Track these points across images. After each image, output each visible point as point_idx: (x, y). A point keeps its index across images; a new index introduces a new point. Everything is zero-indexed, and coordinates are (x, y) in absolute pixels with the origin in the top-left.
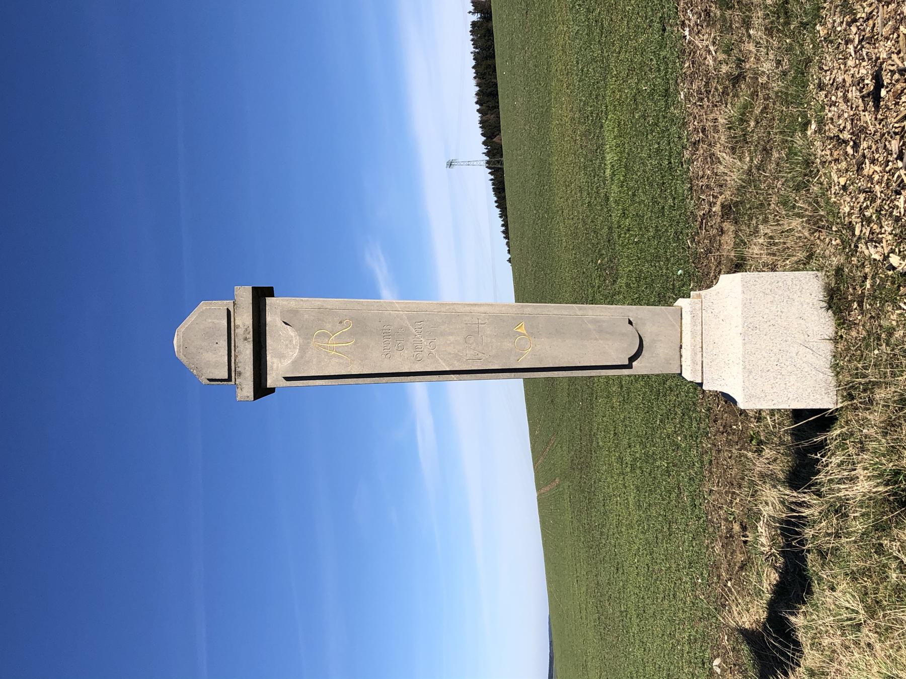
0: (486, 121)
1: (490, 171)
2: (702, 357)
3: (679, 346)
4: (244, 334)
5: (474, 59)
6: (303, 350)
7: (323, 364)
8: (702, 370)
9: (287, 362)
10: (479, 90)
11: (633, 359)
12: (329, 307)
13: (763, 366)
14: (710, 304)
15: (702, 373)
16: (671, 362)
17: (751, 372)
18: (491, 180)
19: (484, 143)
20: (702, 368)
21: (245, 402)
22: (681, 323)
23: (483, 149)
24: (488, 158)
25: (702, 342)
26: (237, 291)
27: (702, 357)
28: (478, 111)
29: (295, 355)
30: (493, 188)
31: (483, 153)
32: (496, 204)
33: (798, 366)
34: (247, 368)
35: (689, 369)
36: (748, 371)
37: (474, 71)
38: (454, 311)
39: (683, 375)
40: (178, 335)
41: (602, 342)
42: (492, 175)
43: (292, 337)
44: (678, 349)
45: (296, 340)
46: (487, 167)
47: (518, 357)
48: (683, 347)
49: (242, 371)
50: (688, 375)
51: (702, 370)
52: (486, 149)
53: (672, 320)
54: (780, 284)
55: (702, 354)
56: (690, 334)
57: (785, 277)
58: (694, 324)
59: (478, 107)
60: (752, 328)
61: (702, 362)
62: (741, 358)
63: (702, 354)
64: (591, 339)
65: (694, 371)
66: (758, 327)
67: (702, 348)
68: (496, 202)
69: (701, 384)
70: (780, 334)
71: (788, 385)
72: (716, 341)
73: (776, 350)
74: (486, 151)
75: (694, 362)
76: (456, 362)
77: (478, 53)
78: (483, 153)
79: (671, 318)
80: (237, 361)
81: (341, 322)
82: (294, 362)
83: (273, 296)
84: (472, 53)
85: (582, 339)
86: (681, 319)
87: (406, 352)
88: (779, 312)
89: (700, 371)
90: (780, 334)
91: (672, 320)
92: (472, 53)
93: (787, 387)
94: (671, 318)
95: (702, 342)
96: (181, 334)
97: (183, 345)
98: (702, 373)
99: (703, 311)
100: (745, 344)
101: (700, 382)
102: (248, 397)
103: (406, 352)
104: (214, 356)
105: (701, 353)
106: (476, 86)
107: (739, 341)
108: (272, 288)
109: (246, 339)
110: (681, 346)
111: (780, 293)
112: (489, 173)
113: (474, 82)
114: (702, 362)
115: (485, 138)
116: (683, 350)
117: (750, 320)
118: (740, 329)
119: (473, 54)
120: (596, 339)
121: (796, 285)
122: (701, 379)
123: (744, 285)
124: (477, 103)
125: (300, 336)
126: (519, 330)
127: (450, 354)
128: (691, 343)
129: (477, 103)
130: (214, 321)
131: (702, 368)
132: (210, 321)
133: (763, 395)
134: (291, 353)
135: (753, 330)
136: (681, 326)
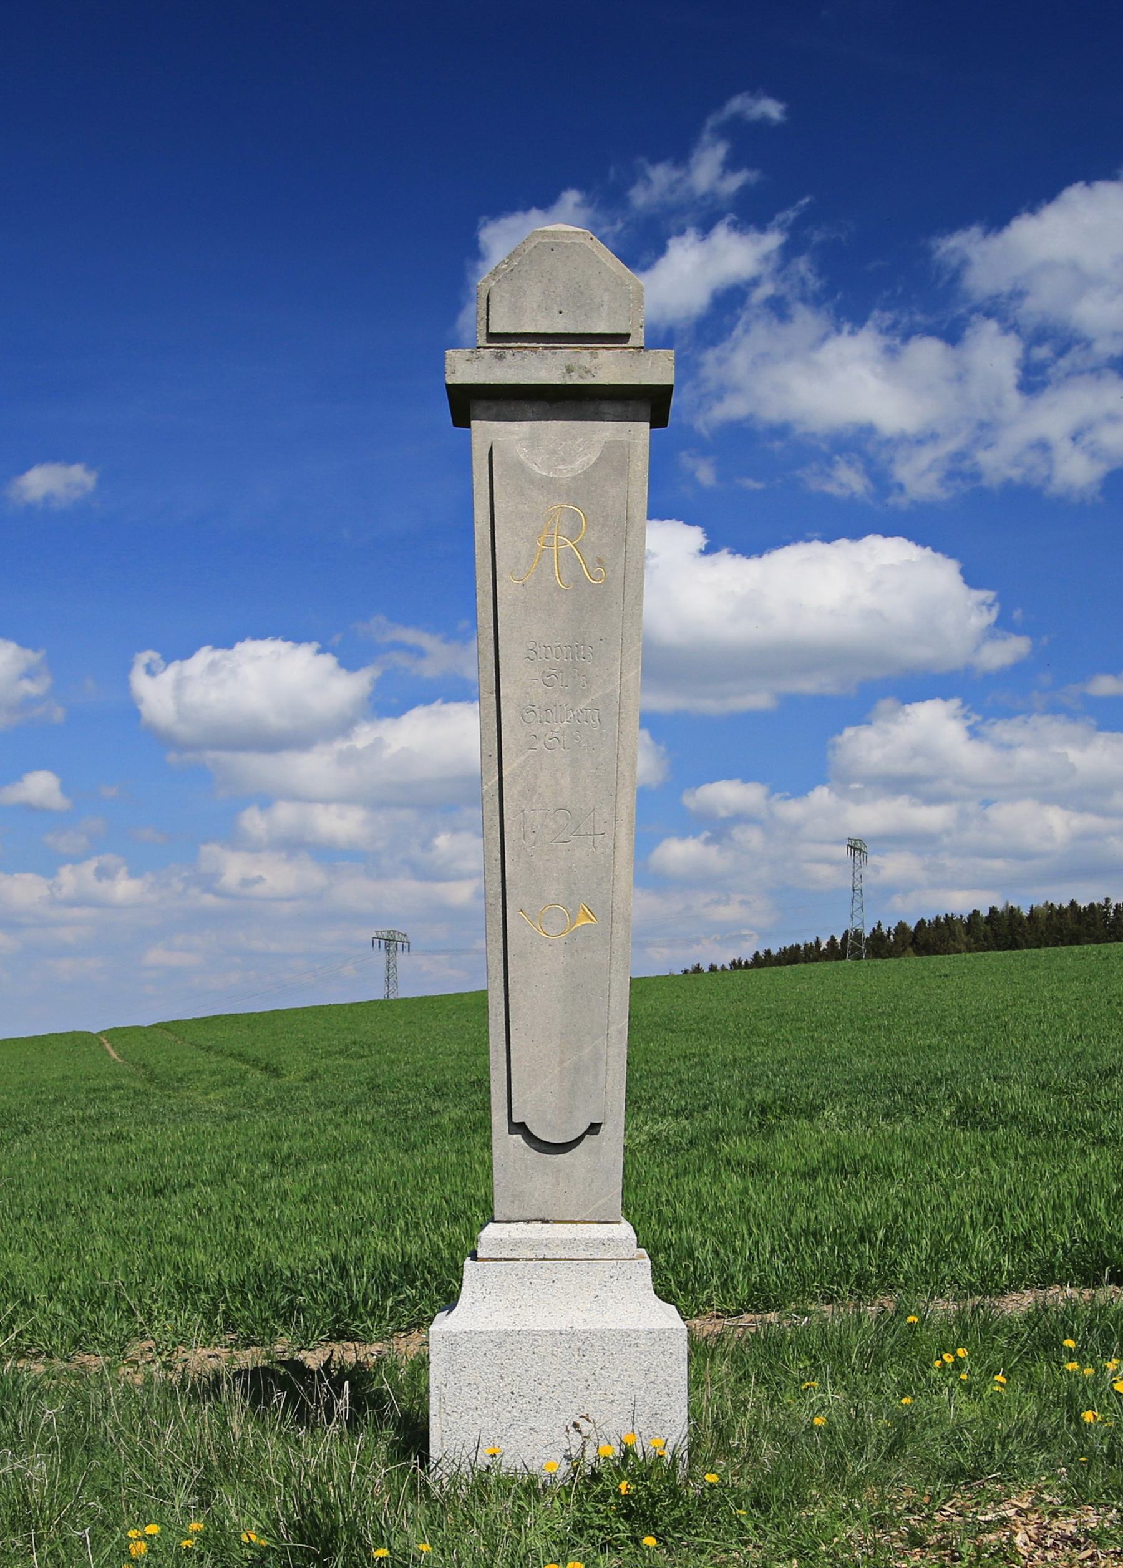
0: (952, 934)
1: (839, 940)
2: (527, 1260)
3: (547, 1218)
4: (581, 367)
5: (1092, 905)
6: (547, 485)
7: (518, 523)
8: (501, 1259)
9: (522, 453)
10: (1021, 917)
11: (520, 1128)
12: (630, 538)
13: (511, 1368)
14: (628, 1274)
15: (496, 1260)
16: (516, 1202)
17: (499, 1345)
18: (818, 943)
19: (901, 928)
20: (506, 1259)
21: (440, 367)
22: (589, 1222)
23: (889, 925)
24: (867, 935)
25: (555, 1259)
26: (665, 354)
27: (527, 1260)
28: (976, 913)
29: (536, 468)
30: (798, 947)
31: (879, 925)
32: (762, 953)
33: (511, 1431)
34: (511, 371)
35: (504, 1236)
36: (502, 1340)
37: (1066, 905)
38: (620, 786)
39: (491, 1225)
40: (577, 233)
41: (556, 1072)
42: (828, 944)
43: (572, 462)
44: (541, 1216)
45: (566, 472)
46: (847, 931)
47: (527, 911)
48: (544, 1225)
49: (506, 362)
50: (491, 1232)
51: (501, 1259)
52: (889, 932)
53: (596, 1205)
54: (665, 1399)
55: (531, 1260)
56: (571, 1236)
57: (677, 1407)
58: (589, 1244)
59: (985, 913)
60: (584, 1348)
61: (518, 1260)
62: (526, 1328)
63: (531, 1260)
64: (562, 1052)
65: (499, 1243)
66: (585, 1359)
67: (544, 1259)
68: (768, 952)
69: (474, 1256)
70: (571, 1398)
71: (475, 1414)
72: (558, 1285)
73: (541, 1391)
74: (884, 930)
75: (517, 1244)
76: (519, 788)
77: (1108, 913)
78: (879, 925)
79: (600, 1202)
80: (526, 352)
81: (600, 561)
82: (521, 467)
83: (651, 428)
84: (1107, 900)
85: (562, 1034)
86: (599, 1222)
87: (540, 691)
88: (612, 1397)
89: (499, 1256)
90: (571, 1398)
91: (596, 1205)
92: (1107, 900)
93: (471, 1412)
94: (600, 1202)
95: (555, 1259)
96: (579, 240)
97: (557, 244)
98: (496, 1260)
99: (614, 1261)
100: (552, 1334)
101: (479, 1256)
102: (453, 373)
103: (540, 691)
104: (535, 306)
105: (533, 1256)
106: (1032, 910)
107: (562, 1325)
108: (455, 425)
109: (569, 370)
110: (547, 1222)
111: (649, 1400)
112: (833, 938)
113: (1039, 903)
114: (518, 1260)
115: (913, 929)
116: (539, 1225)
117: (598, 1344)
118: (579, 1326)
119: (1103, 903)
120: (562, 1062)
121: (662, 1428)
122: (485, 1257)
123: (664, 1333)
124: (993, 910)
125: (574, 478)
126: (581, 914)
127: (536, 777)
128: (553, 1240)
129: (993, 910)
130: (606, 307)
131: (506, 1259)
132: (606, 299)
133: (455, 1368)
134: (539, 460)
135: (579, 1349)
136: (585, 1222)
